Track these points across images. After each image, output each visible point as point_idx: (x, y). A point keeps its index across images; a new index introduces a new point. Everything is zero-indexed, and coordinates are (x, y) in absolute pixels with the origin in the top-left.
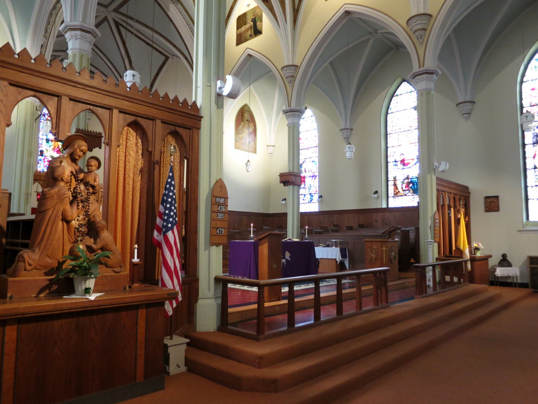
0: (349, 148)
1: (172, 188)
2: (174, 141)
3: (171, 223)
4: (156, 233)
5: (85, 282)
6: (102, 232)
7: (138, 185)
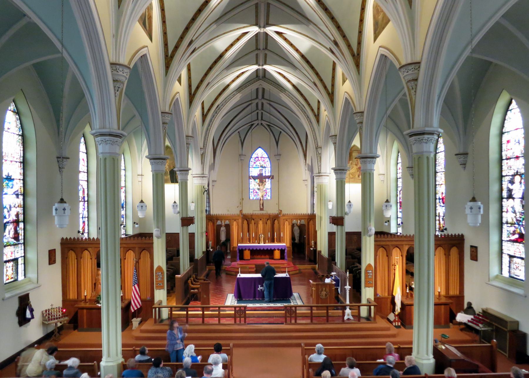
0: (471, 208)
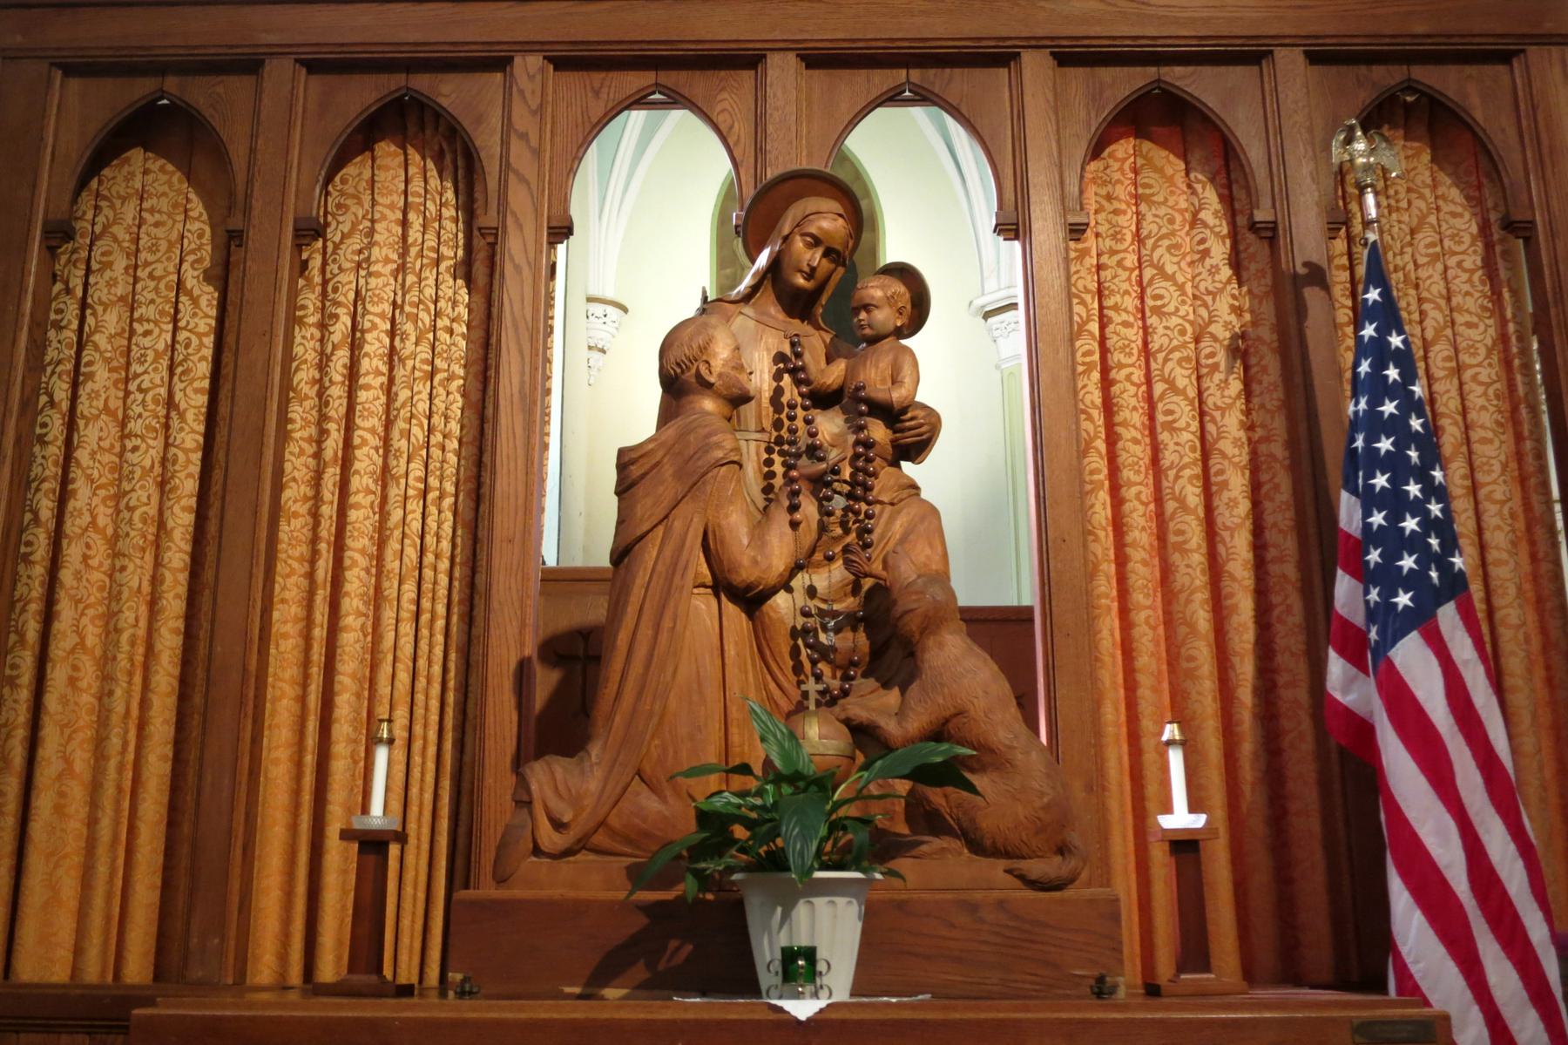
1: (1393, 373)
2: (1426, 157)
3: (1412, 581)
4: (1336, 666)
5: (786, 916)
6: (930, 642)
7: (1230, 426)
